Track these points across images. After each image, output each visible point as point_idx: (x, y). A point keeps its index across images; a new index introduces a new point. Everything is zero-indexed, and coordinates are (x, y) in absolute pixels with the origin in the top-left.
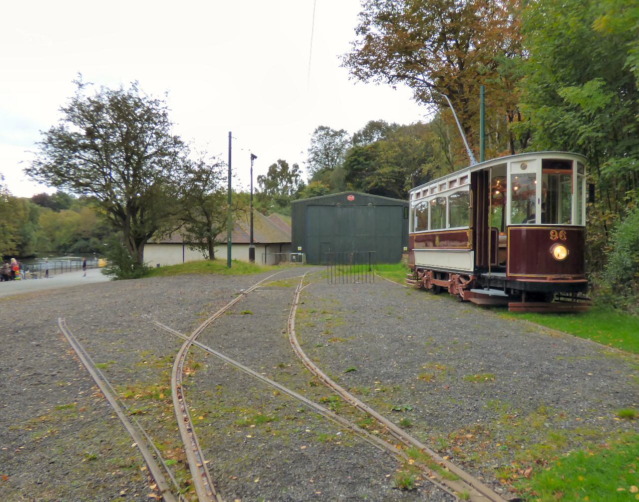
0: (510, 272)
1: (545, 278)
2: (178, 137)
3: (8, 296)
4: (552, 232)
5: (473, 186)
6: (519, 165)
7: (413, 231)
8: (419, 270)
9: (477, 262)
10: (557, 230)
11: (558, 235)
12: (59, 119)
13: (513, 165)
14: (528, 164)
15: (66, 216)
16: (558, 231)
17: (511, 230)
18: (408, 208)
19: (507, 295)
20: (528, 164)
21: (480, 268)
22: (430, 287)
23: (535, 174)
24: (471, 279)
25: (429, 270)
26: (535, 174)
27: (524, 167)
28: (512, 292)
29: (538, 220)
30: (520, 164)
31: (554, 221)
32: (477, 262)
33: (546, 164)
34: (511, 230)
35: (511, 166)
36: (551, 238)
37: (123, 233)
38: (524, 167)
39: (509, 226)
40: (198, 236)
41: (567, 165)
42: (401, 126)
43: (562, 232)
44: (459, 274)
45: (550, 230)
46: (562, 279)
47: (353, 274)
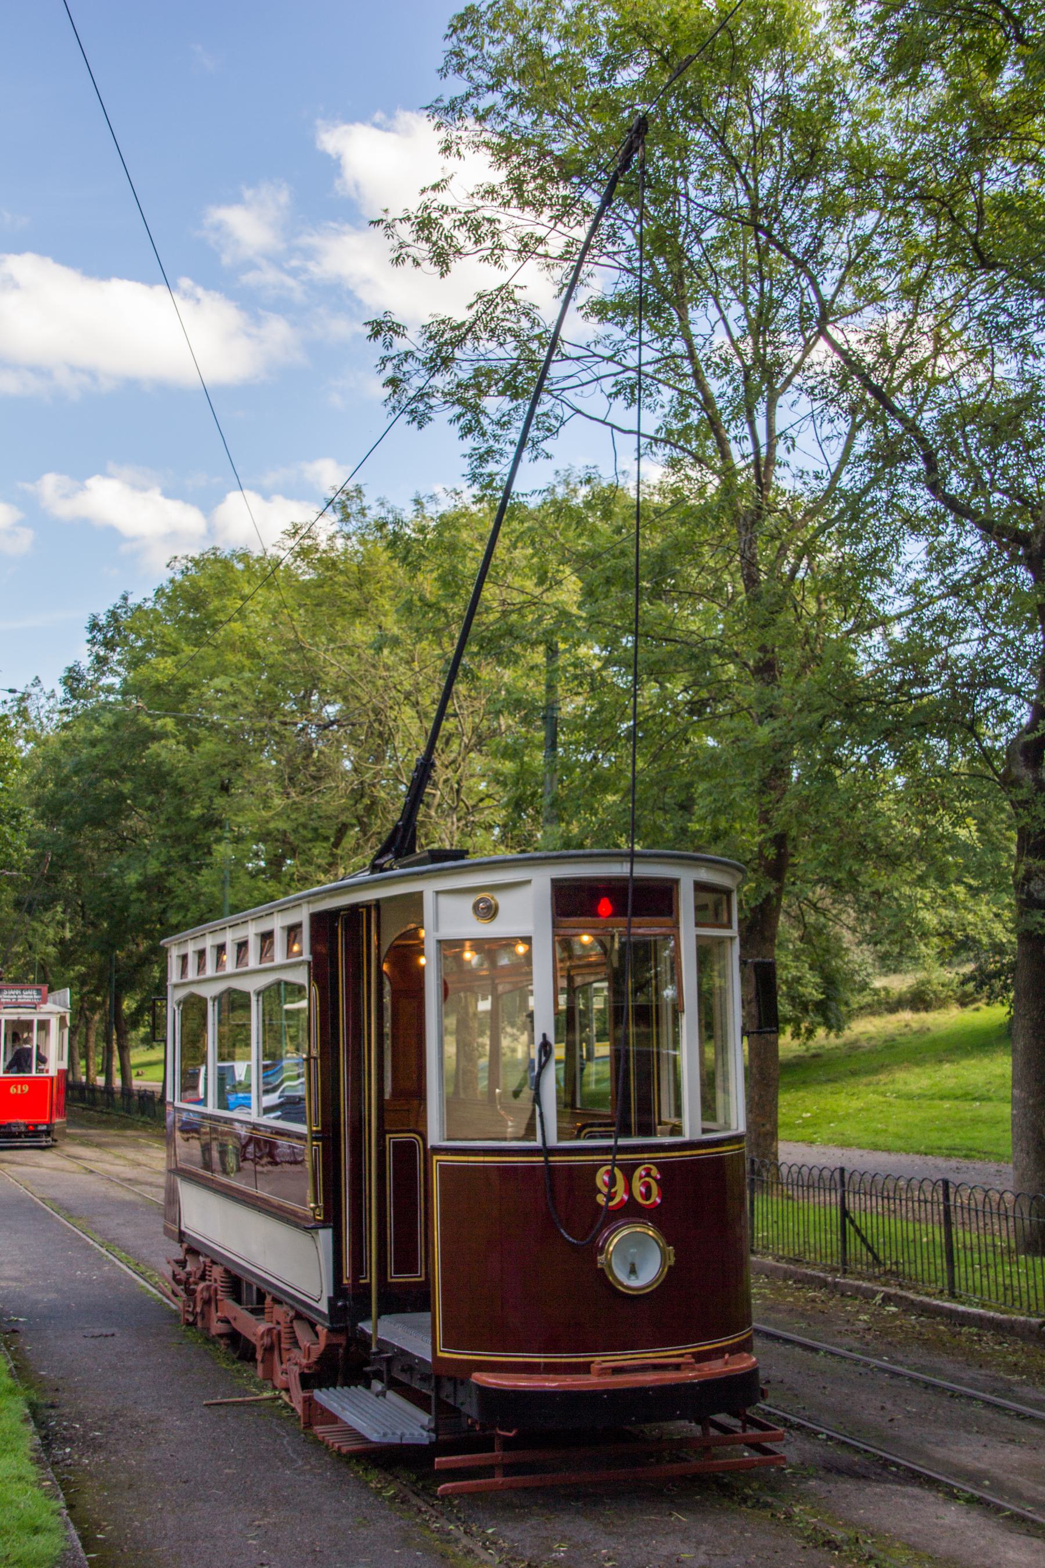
1: (585, 1368)
4: (601, 1178)
5: (322, 970)
9: (347, 1271)
10: (621, 1167)
11: (629, 1190)
12: (452, 185)
13: (443, 900)
14: (502, 900)
16: (629, 1171)
17: (443, 1169)
18: (666, 1420)
21: (349, 1302)
23: (553, 881)
26: (553, 881)
27: (488, 912)
30: (469, 901)
32: (347, 1271)
33: (571, 901)
34: (443, 1169)
36: (601, 1199)
37: (621, 1274)
39: (437, 1150)
41: (658, 899)
43: (640, 1171)
44: (292, 1307)
45: (596, 1168)
46: (657, 1367)
47: (929, 1206)
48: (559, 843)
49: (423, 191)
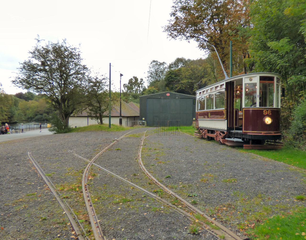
0: (244, 130)
1: (261, 133)
3: (4, 142)
4: (264, 111)
5: (227, 89)
6: (248, 79)
7: (198, 110)
8: (201, 129)
9: (228, 125)
10: (267, 110)
11: (267, 113)
12: (28, 57)
13: (246, 79)
14: (253, 78)
16: (267, 111)
17: (244, 110)
19: (243, 141)
20: (253, 78)
21: (230, 128)
22: (206, 137)
24: (226, 134)
25: (205, 129)
27: (251, 80)
28: (245, 140)
30: (249, 78)
31: (265, 106)
32: (228, 125)
33: (262, 78)
34: (244, 110)
35: (245, 79)
36: (264, 114)
38: (251, 80)
39: (244, 108)
41: (271, 79)
43: (269, 111)
44: (220, 131)
45: (263, 110)
46: (269, 133)
48: (98, 229)
49: (29, 57)
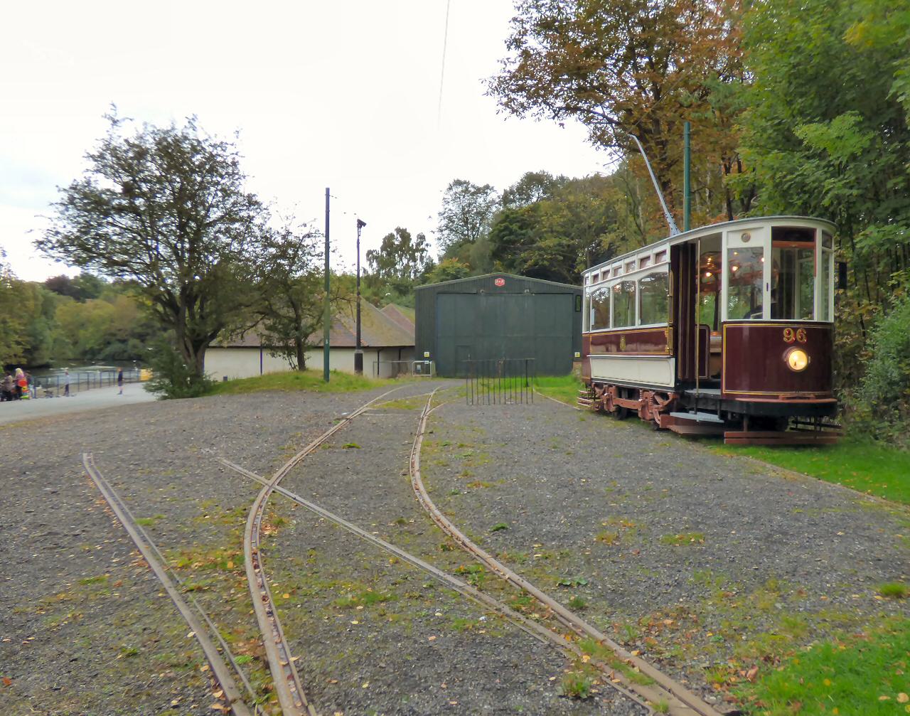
0: (727, 388)
1: (777, 397)
2: (254, 195)
3: (11, 422)
4: (785, 332)
5: (674, 265)
6: (739, 236)
7: (588, 329)
8: (597, 385)
9: (679, 374)
10: (793, 329)
11: (795, 336)
12: (85, 169)
13: (731, 235)
14: (752, 234)
15: (94, 308)
16: (795, 330)
17: (727, 329)
19: (722, 421)
20: (752, 234)
21: (683, 382)
22: (613, 409)
23: (762, 248)
24: (671, 398)
25: (610, 386)
26: (762, 248)
27: (746, 238)
28: (729, 416)
29: (766, 314)
30: (741, 234)
31: (789, 315)
32: (679, 374)
33: (778, 234)
34: (727, 329)
35: (728, 237)
36: (785, 339)
38: (746, 238)
39: (725, 323)
40: (282, 336)
41: (807, 235)
42: (571, 179)
43: (800, 330)
44: (654, 391)
45: (783, 329)
46: (800, 398)
48: (292, 683)
49: (88, 170)
